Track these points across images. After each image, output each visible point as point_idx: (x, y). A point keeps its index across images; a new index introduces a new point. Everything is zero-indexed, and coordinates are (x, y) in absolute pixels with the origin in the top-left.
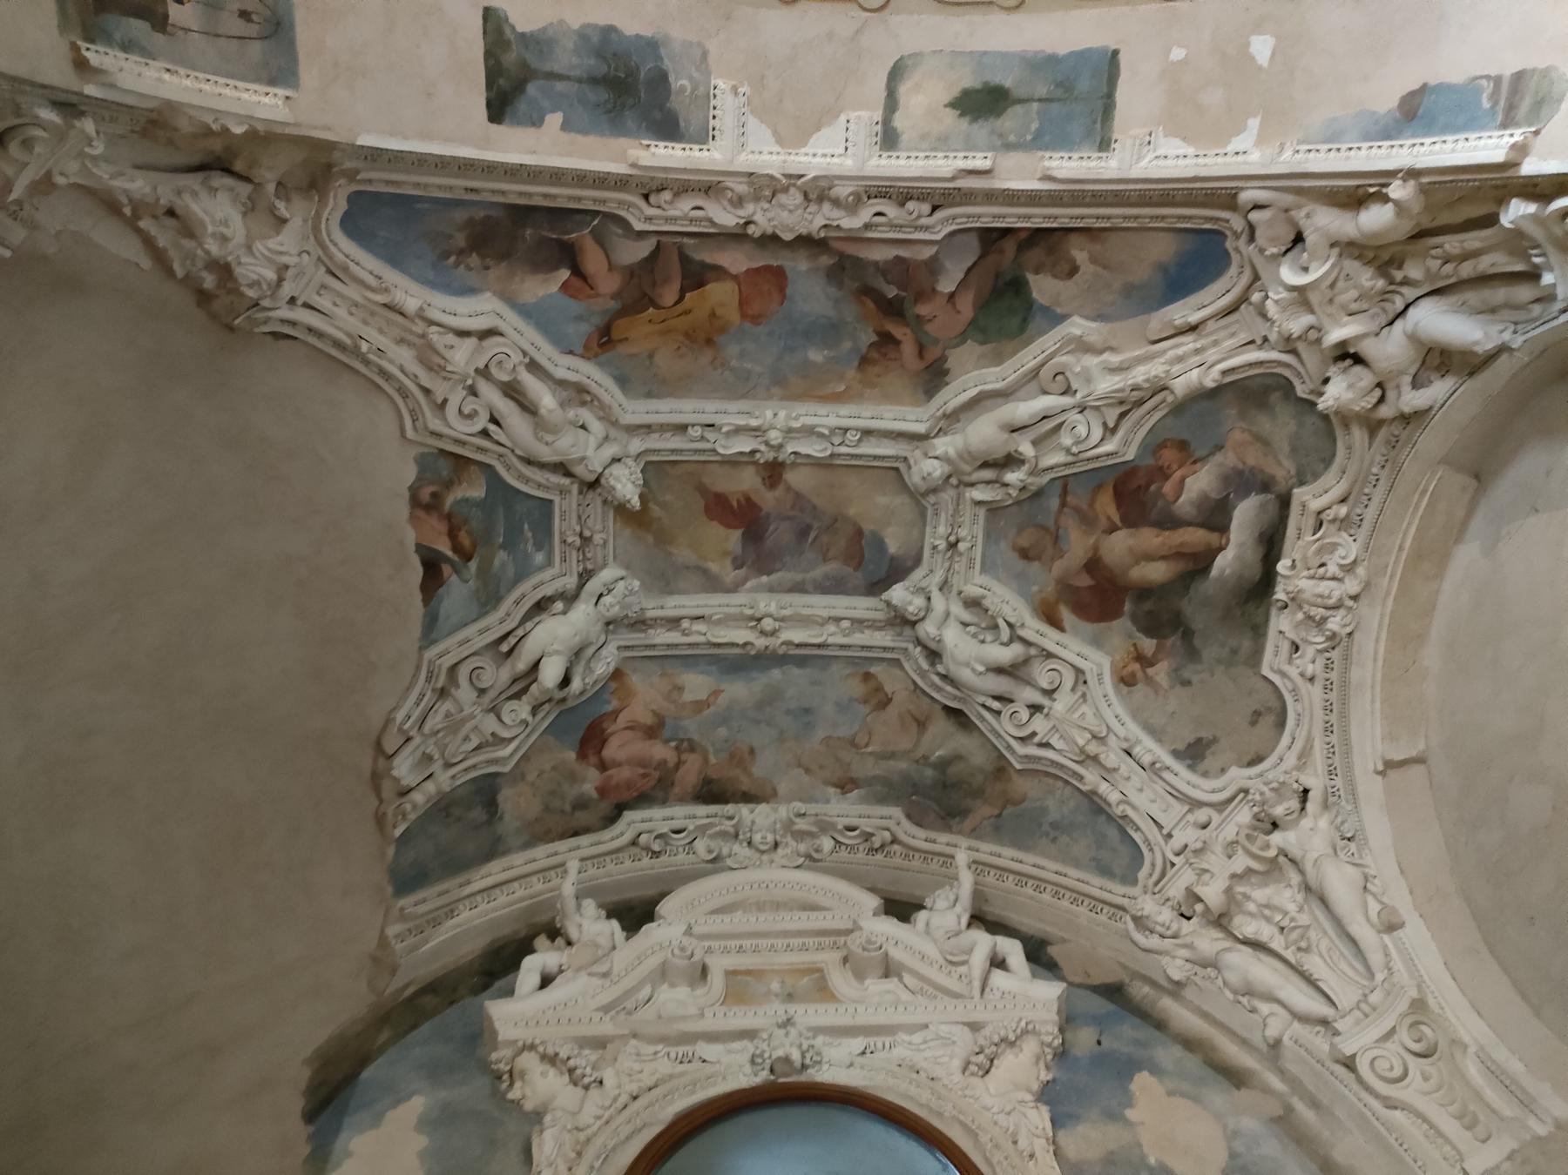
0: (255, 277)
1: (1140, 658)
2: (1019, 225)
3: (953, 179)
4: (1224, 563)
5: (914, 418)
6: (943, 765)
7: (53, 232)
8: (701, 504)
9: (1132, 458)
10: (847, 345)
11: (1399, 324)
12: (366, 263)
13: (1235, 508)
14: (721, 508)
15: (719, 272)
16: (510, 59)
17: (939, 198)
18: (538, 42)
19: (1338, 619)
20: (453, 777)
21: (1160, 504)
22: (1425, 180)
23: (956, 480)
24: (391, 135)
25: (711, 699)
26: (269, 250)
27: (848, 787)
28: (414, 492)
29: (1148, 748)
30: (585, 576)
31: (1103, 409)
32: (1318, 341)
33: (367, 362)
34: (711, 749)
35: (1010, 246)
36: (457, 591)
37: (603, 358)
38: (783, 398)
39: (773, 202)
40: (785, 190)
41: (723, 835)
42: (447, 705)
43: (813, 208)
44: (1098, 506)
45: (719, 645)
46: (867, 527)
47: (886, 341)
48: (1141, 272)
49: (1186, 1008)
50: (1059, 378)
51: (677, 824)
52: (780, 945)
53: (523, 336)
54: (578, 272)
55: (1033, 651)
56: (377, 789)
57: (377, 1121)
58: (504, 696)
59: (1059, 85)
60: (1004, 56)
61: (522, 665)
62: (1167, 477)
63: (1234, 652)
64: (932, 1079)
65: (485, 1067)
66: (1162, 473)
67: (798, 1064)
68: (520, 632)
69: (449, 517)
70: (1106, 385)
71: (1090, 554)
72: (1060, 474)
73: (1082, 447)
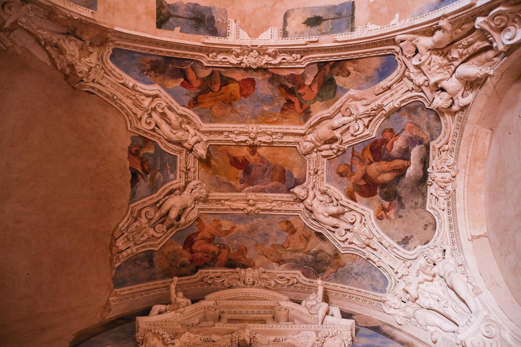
0: (81, 70)
3: (306, 44)
4: (410, 171)
5: (300, 129)
6: (315, 254)
8: (228, 160)
9: (374, 136)
10: (277, 104)
11: (454, 76)
12: (118, 71)
13: (411, 151)
14: (236, 162)
15: (233, 80)
16: (164, 11)
17: (304, 52)
18: (173, 7)
19: (450, 186)
20: (137, 249)
21: (386, 152)
23: (315, 149)
25: (232, 230)
26: (86, 61)
27: (281, 263)
28: (130, 148)
29: (387, 240)
30: (187, 183)
31: (362, 119)
33: (116, 103)
34: (231, 248)
35: (328, 67)
36: (143, 185)
37: (195, 108)
38: (256, 123)
40: (252, 51)
41: (235, 278)
42: (137, 223)
44: (365, 155)
45: (234, 210)
46: (286, 169)
47: (289, 102)
48: (370, 72)
50: (347, 110)
51: (218, 275)
52: (250, 312)
53: (166, 98)
54: (186, 79)
55: (346, 210)
56: (111, 251)
59: (337, 14)
60: (320, 7)
61: (163, 211)
62: (387, 142)
63: (416, 204)
65: (134, 339)
67: (248, 342)
69: (141, 159)
70: (362, 110)
71: (364, 173)
72: (351, 145)
73: (357, 133)
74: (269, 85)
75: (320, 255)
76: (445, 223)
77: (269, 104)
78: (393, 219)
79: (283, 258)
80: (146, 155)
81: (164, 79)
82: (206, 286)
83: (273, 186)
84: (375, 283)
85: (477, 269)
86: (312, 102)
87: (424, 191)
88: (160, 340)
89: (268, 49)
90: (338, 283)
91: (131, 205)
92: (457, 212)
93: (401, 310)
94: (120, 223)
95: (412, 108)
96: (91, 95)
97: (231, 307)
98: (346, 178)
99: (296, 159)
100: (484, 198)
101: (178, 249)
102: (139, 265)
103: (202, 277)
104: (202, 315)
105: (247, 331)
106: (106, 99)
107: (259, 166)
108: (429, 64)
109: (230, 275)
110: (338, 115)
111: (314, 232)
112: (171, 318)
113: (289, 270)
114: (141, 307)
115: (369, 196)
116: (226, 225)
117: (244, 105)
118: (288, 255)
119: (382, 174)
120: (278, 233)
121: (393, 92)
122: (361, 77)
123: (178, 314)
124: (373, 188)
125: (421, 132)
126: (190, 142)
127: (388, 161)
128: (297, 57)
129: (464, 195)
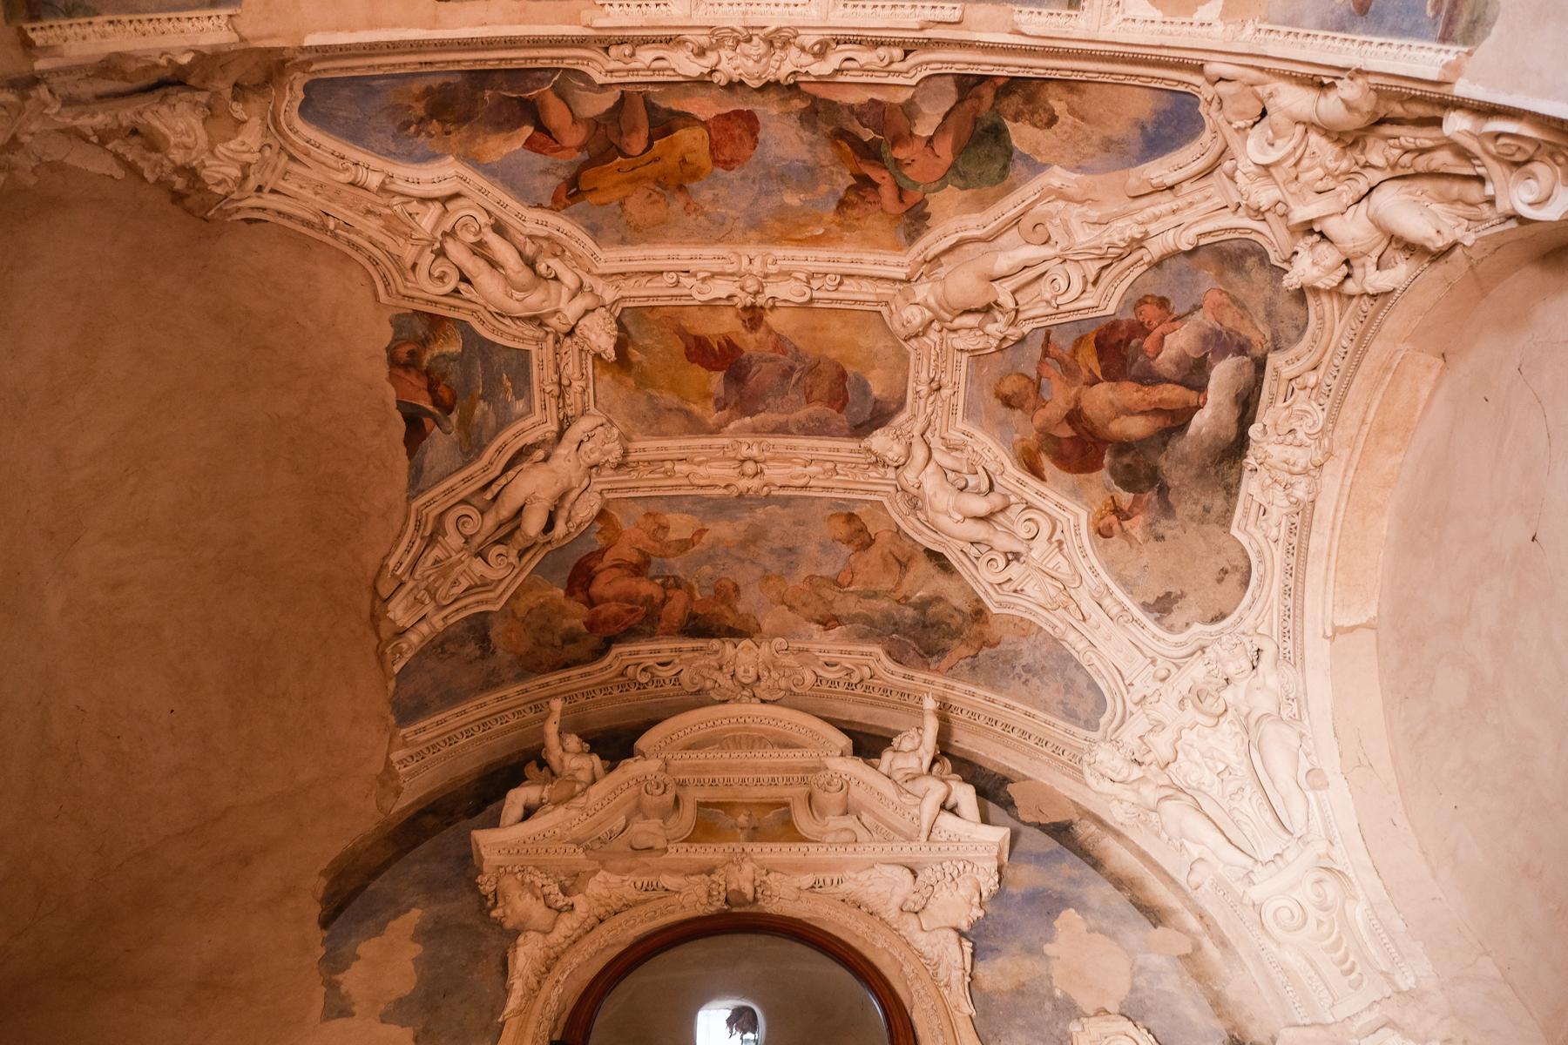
0: (220, 177)
1: (1117, 511)
2: (995, 73)
4: (1201, 422)
5: (896, 264)
6: (923, 606)
7: (30, 169)
8: (680, 347)
10: (825, 188)
12: (330, 143)
13: (1211, 368)
14: (701, 351)
15: (688, 119)
22: (1373, 80)
24: (338, 30)
25: (696, 538)
27: (830, 624)
32: (1285, 215)
34: (696, 586)
36: (440, 444)
37: (572, 208)
38: (761, 242)
39: (738, 51)
42: (437, 552)
43: (779, 54)
44: (1080, 359)
46: (851, 370)
47: (864, 184)
48: (1119, 128)
49: (1126, 848)
50: (1038, 228)
54: (541, 127)
56: (376, 629)
57: (380, 929)
58: (491, 540)
61: (506, 510)
62: (1148, 333)
63: (1207, 510)
64: (871, 914)
65: (474, 887)
66: (1140, 329)
67: (750, 896)
68: (503, 481)
69: (427, 373)
70: (1084, 237)
71: (1072, 406)
73: (1060, 300)
74: (802, 133)
75: (934, 609)
76: (1272, 577)
77: (800, 187)
78: (1139, 540)
79: (836, 612)
80: (441, 360)
81: (471, 139)
82: (633, 690)
83: (810, 418)
84: (1072, 700)
85: (1330, 717)
86: (934, 186)
87: (1230, 480)
88: (537, 898)
89: (799, 35)
90: (977, 685)
91: (416, 504)
92: (1309, 559)
93: (1128, 787)
94: (389, 555)
95: (1229, 253)
96: (254, 226)
97: (697, 769)
98: (1019, 411)
99: (880, 345)
100: (1389, 528)
101: (552, 598)
102: (453, 654)
103: (622, 667)
104: (632, 804)
105: (748, 868)
106: (305, 230)
107: (771, 360)
108: (1296, 165)
109: (696, 658)
110: (1010, 232)
111: (922, 550)
112: (557, 825)
113: (851, 642)
114: (473, 766)
115: (1079, 471)
116: (680, 525)
117: (723, 192)
118: (847, 605)
119: (1123, 417)
120: (824, 548)
121: (1180, 203)
122: (1088, 138)
123: (573, 813)
124: (1094, 450)
125: (1246, 323)
126: (565, 316)
127: (1143, 385)
128: (891, 57)
129: (1335, 518)
